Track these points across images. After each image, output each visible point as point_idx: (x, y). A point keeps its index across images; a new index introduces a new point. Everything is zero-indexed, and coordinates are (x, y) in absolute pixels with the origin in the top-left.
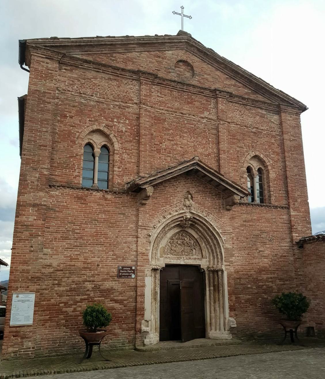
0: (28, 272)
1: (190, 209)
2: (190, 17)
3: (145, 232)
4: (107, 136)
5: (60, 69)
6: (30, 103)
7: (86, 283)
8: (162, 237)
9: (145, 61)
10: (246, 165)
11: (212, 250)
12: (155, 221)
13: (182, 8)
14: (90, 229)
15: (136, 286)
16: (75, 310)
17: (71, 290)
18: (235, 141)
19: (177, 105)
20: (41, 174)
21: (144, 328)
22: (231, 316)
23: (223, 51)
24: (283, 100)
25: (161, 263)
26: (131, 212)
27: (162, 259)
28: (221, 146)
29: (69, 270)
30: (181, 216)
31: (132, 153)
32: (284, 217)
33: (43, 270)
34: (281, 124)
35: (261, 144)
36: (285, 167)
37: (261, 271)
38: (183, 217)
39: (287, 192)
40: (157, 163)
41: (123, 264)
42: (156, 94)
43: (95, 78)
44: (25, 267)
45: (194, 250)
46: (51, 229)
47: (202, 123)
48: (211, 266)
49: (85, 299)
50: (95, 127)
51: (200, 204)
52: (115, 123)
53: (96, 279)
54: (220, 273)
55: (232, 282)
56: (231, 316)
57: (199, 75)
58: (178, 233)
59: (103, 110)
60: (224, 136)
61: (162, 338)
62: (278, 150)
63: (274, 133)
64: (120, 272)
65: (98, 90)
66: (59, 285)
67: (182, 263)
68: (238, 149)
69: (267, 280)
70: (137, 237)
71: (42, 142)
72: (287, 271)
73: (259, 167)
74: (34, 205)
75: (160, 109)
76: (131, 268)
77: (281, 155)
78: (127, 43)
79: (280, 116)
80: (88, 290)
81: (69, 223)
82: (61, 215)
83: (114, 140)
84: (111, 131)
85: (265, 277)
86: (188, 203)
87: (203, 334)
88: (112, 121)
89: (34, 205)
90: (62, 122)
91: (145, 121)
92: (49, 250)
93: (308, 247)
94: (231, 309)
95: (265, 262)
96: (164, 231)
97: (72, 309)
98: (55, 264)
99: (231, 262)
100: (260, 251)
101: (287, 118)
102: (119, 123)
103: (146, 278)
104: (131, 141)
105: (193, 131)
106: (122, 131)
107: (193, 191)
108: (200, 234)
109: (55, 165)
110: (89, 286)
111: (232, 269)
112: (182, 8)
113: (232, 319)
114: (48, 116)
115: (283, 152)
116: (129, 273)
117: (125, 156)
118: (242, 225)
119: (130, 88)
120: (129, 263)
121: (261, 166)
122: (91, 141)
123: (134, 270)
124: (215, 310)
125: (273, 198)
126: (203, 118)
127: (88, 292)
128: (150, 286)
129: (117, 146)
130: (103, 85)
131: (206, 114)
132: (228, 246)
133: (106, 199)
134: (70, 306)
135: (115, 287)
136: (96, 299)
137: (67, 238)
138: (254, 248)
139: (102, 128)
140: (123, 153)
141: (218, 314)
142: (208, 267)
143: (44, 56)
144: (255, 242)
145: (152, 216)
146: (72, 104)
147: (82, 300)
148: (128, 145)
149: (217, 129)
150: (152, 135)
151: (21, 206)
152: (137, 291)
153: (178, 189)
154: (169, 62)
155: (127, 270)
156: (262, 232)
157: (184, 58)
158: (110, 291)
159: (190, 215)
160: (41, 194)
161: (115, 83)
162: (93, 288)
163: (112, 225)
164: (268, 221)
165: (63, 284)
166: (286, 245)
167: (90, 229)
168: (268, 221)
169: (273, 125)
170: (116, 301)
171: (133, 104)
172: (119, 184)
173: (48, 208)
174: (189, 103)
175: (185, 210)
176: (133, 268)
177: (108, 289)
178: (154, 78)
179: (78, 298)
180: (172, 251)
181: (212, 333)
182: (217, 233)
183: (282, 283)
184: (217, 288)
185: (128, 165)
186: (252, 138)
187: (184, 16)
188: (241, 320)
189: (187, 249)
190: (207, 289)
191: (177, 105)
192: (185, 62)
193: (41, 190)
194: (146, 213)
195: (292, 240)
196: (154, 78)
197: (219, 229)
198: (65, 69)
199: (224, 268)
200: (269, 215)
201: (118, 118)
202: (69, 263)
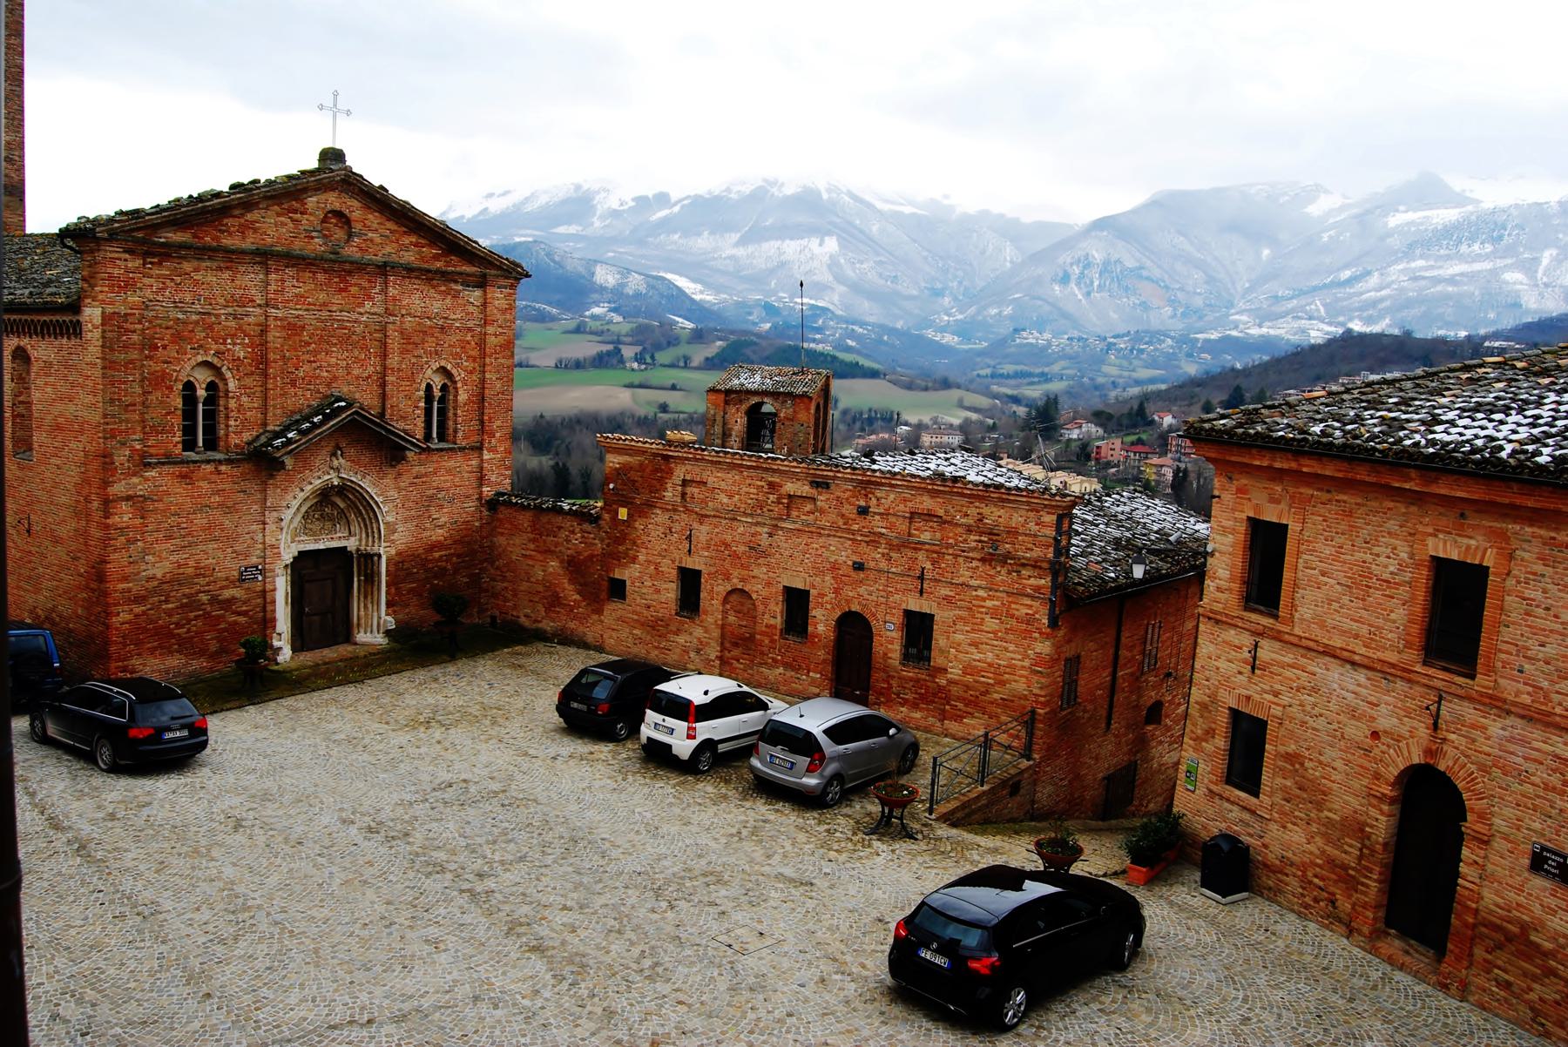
3: (275, 514)
4: (216, 370)
9: (273, 228)
12: (289, 497)
13: (336, 94)
14: (200, 520)
15: (264, 591)
16: (189, 631)
17: (183, 606)
19: (322, 296)
20: (133, 450)
21: (276, 643)
26: (252, 486)
28: (388, 362)
29: (175, 580)
34: (485, 305)
36: (483, 381)
37: (433, 547)
39: (482, 422)
40: (290, 403)
41: (245, 563)
42: (292, 284)
43: (197, 270)
50: (200, 359)
57: (360, 235)
59: (211, 327)
60: (394, 342)
61: (294, 650)
62: (475, 353)
63: (470, 324)
66: (167, 602)
67: (322, 547)
70: (264, 523)
71: (129, 400)
72: (469, 543)
78: (248, 197)
82: (160, 506)
83: (228, 375)
85: (437, 555)
86: (336, 463)
87: (348, 638)
88: (224, 343)
89: (128, 498)
91: (275, 336)
93: (504, 513)
94: (388, 605)
95: (439, 534)
98: (159, 575)
99: (393, 542)
102: (234, 344)
105: (346, 341)
110: (204, 598)
113: (389, 618)
114: (134, 355)
115: (483, 355)
117: (244, 399)
119: (250, 280)
120: (254, 560)
125: (460, 434)
128: (282, 587)
129: (232, 385)
130: (213, 282)
132: (390, 519)
133: (219, 473)
145: (285, 490)
146: (164, 323)
147: (196, 618)
148: (248, 381)
149: (383, 330)
152: (266, 598)
157: (337, 206)
158: (232, 600)
160: (135, 480)
161: (226, 275)
163: (229, 509)
164: (449, 471)
166: (471, 505)
167: (200, 520)
168: (449, 471)
169: (471, 309)
170: (239, 614)
172: (236, 446)
173: (145, 498)
174: (341, 290)
175: (333, 474)
178: (291, 260)
179: (192, 615)
180: (306, 530)
181: (362, 637)
184: (371, 578)
188: (400, 616)
189: (328, 525)
191: (322, 296)
192: (339, 214)
193: (134, 474)
194: (277, 487)
195: (480, 499)
196: (291, 260)
200: (451, 463)
201: (233, 336)
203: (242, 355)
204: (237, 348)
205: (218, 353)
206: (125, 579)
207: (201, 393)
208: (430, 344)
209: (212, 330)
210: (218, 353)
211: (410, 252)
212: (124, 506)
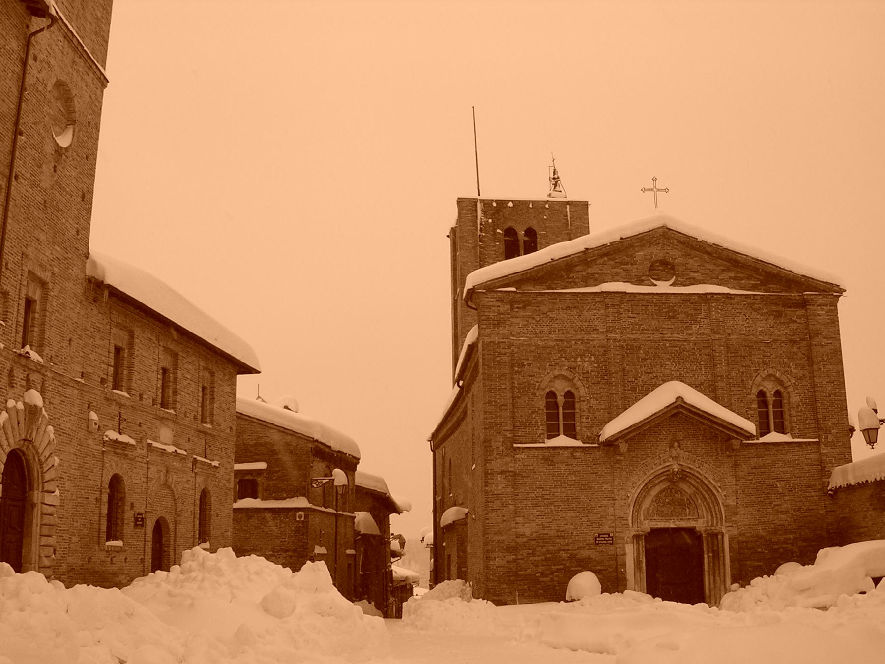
0: (503, 541)
2: (666, 190)
5: (512, 310)
6: (458, 230)
7: (561, 552)
8: (645, 496)
10: (755, 391)
11: (710, 508)
12: (634, 478)
18: (738, 359)
20: (505, 437)
25: (647, 526)
27: (646, 522)
30: (667, 469)
31: (601, 398)
32: (812, 456)
33: (518, 540)
41: (600, 531)
43: (551, 311)
44: (501, 538)
46: (521, 496)
47: (690, 341)
49: (561, 569)
50: (556, 373)
53: (570, 548)
54: (720, 536)
55: (736, 546)
58: (665, 489)
66: (534, 554)
67: (672, 526)
68: (744, 370)
69: (785, 542)
71: (502, 402)
73: (775, 389)
74: (502, 472)
77: (807, 367)
82: (528, 480)
83: (579, 384)
89: (502, 472)
90: (519, 373)
92: (521, 519)
96: (646, 489)
97: (548, 579)
98: (528, 533)
103: (627, 546)
107: (681, 435)
109: (518, 424)
110: (564, 555)
111: (735, 532)
112: (655, 179)
117: (593, 402)
118: (750, 473)
120: (606, 529)
122: (553, 389)
124: (715, 581)
129: (583, 392)
131: (695, 328)
134: (546, 576)
135: (593, 556)
137: (537, 505)
138: (768, 501)
139: (564, 373)
141: (718, 585)
147: (558, 570)
150: (624, 370)
159: (679, 467)
160: (508, 459)
165: (538, 553)
173: (515, 474)
174: (670, 318)
176: (611, 535)
182: (715, 487)
184: (717, 555)
186: (764, 351)
187: (659, 190)
190: (706, 556)
197: (717, 481)
199: (724, 531)
201: (582, 356)
202: (542, 532)
203: (590, 369)
204: (586, 364)
205: (570, 368)
206: (499, 533)
207: (561, 400)
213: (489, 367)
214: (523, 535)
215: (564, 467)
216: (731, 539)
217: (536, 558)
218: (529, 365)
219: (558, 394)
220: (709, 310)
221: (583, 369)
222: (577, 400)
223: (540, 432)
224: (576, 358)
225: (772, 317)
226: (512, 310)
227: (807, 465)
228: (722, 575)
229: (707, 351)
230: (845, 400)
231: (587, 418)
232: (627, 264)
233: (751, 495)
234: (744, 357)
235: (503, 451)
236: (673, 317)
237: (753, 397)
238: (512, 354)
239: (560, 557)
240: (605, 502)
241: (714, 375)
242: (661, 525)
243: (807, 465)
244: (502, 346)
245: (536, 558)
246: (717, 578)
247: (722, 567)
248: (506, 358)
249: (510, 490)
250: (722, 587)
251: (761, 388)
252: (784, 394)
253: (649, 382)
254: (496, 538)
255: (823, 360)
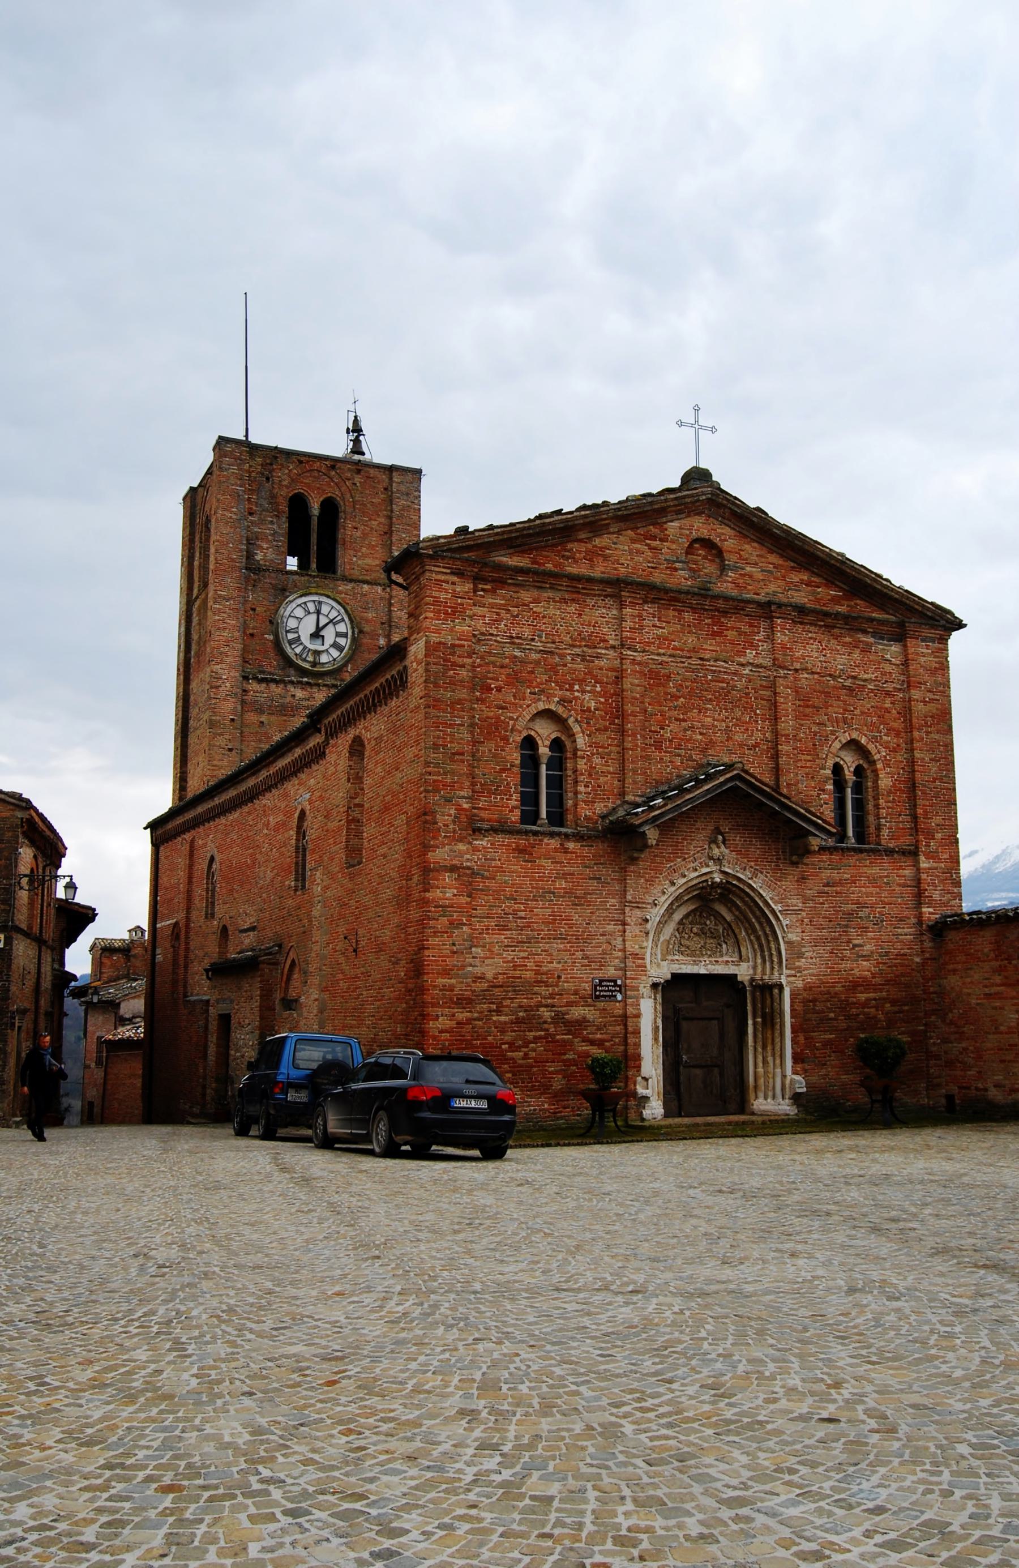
1: (721, 865)
5: (475, 591)
9: (625, 555)
10: (830, 763)
11: (761, 946)
12: (656, 891)
13: (697, 409)
16: (526, 1056)
18: (808, 710)
19: (691, 640)
20: (459, 809)
22: (795, 1073)
23: (784, 512)
24: (911, 610)
27: (665, 963)
30: (704, 878)
31: (609, 754)
35: (863, 713)
38: (706, 881)
39: (915, 817)
41: (600, 974)
43: (536, 601)
45: (724, 946)
47: (742, 676)
48: (758, 977)
50: (541, 706)
51: (739, 852)
52: (576, 694)
54: (776, 991)
55: (799, 1008)
56: (795, 1073)
58: (692, 911)
59: (554, 669)
64: (596, 990)
65: (543, 627)
66: (498, 1012)
67: (703, 971)
68: (815, 728)
69: (866, 1004)
71: (455, 747)
74: (453, 869)
75: (659, 654)
76: (615, 981)
77: (903, 734)
79: (905, 646)
80: (545, 1022)
81: (508, 899)
83: (576, 728)
84: (570, 711)
85: (862, 997)
88: (571, 690)
89: (453, 869)
92: (479, 950)
94: (797, 1058)
96: (670, 911)
98: (489, 975)
100: (855, 946)
101: (921, 651)
104: (606, 729)
106: (589, 710)
108: (737, 913)
110: (546, 1014)
111: (800, 984)
112: (697, 409)
116: (612, 991)
117: (597, 760)
120: (611, 972)
121: (861, 762)
122: (533, 733)
123: (620, 986)
124: (765, 1062)
126: (743, 665)
127: (546, 1026)
129: (581, 741)
131: (750, 655)
133: (566, 851)
134: (518, 1049)
135: (590, 1017)
136: (558, 1037)
137: (504, 928)
138: (845, 938)
140: (593, 754)
142: (752, 980)
143: (448, 571)
144: (847, 926)
146: (500, 661)
147: (536, 1039)
148: (601, 738)
151: (432, 870)
152: (627, 1024)
153: (698, 825)
154: (674, 546)
155: (608, 986)
156: (862, 906)
157: (704, 533)
160: (462, 847)
162: (552, 1018)
164: (873, 881)
166: (907, 932)
168: (873, 881)
169: (888, 668)
170: (592, 1043)
171: (606, 648)
174: (715, 634)
176: (619, 982)
177: (577, 1021)
182: (773, 912)
183: (896, 1009)
184: (770, 1020)
185: (602, 780)
190: (750, 1022)
191: (691, 640)
193: (461, 840)
197: (776, 903)
198: (483, 590)
200: (875, 871)
201: (582, 682)
203: (593, 705)
204: (587, 696)
205: (562, 701)
206: (446, 973)
207: (544, 751)
208: (835, 710)
209: (556, 673)
210: (562, 701)
211: (801, 590)
212: (448, 878)
213: (436, 685)
214: (482, 978)
215: (547, 863)
216: (794, 996)
217: (503, 1018)
218: (499, 689)
219: (540, 742)
220: (772, 628)
221: (582, 705)
222: (569, 755)
223: (514, 803)
224: (572, 686)
225: (858, 651)
226: (475, 591)
227: (899, 885)
228: (778, 1054)
229: (766, 693)
230: (954, 790)
231: (586, 786)
232: (654, 538)
233: (820, 928)
234: (818, 709)
235: (454, 831)
236: (719, 634)
237: (828, 772)
238: (474, 666)
239: (540, 1017)
240: (610, 928)
241: (776, 733)
242: (702, 968)
243: (899, 885)
244: (459, 651)
245: (503, 1018)
246: (770, 1059)
247: (777, 1040)
248: (464, 673)
249: (464, 900)
250: (778, 1071)
251: (838, 760)
252: (869, 773)
253: (680, 735)
254: (441, 981)
255: (926, 725)
